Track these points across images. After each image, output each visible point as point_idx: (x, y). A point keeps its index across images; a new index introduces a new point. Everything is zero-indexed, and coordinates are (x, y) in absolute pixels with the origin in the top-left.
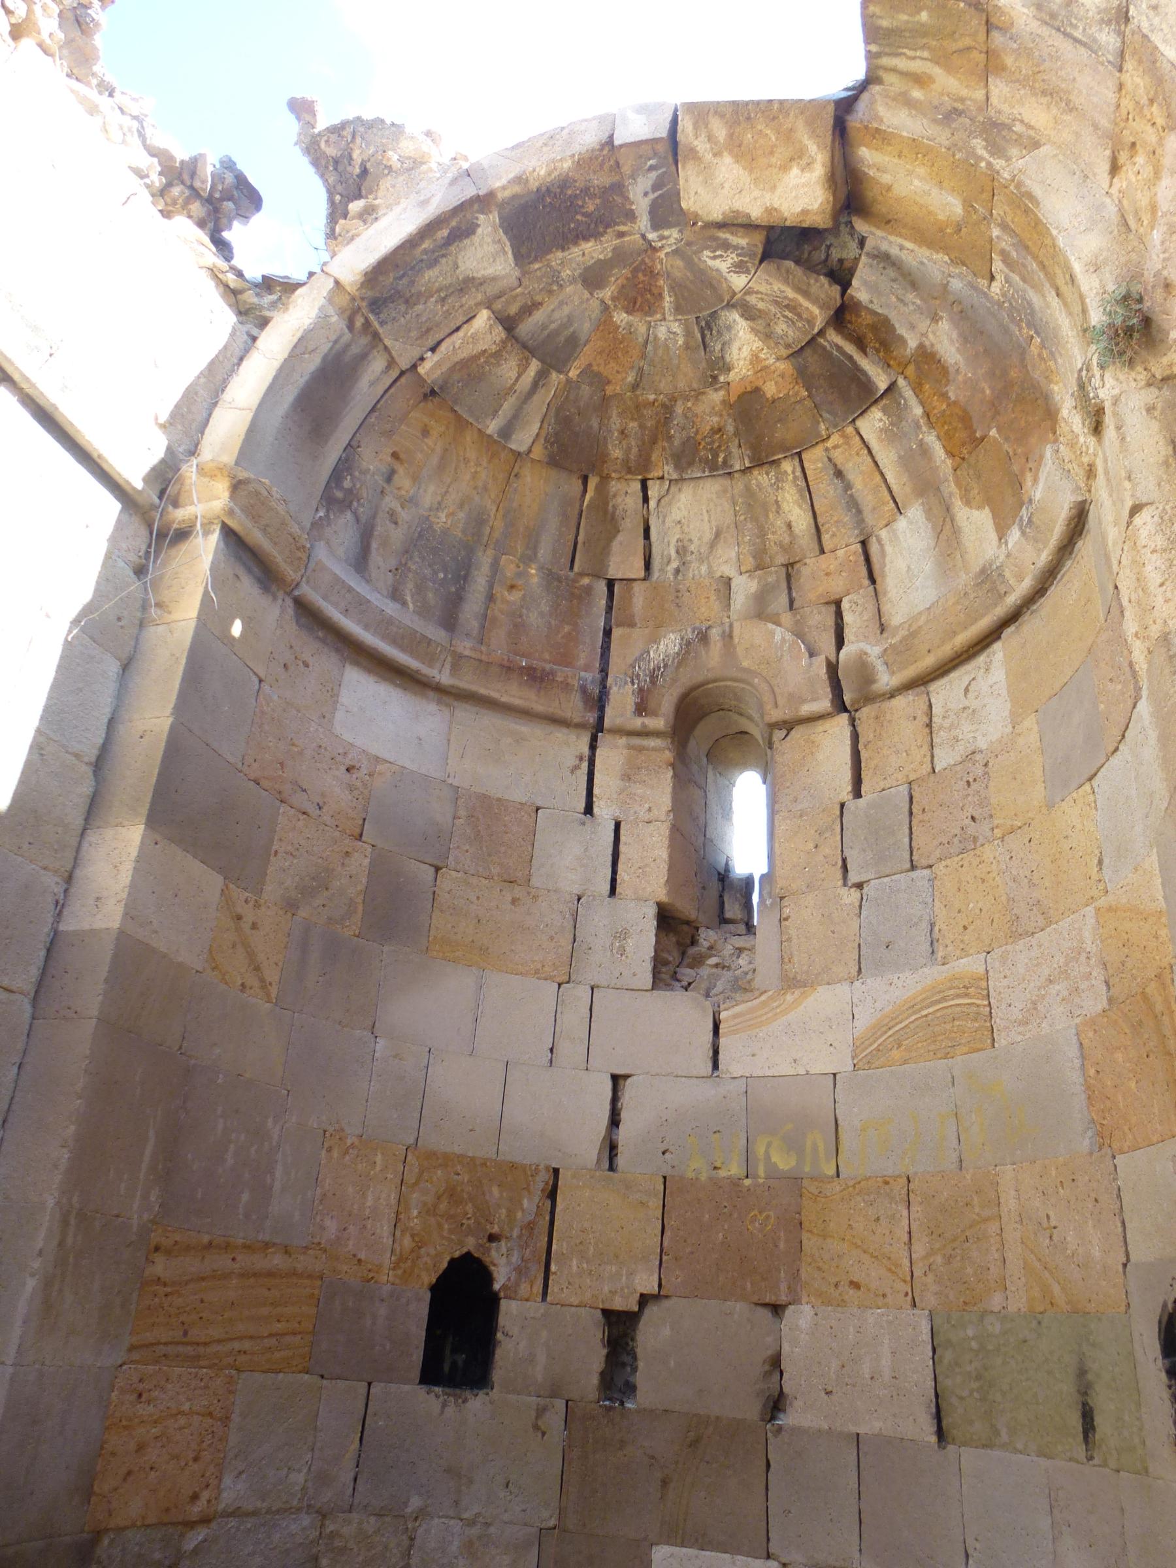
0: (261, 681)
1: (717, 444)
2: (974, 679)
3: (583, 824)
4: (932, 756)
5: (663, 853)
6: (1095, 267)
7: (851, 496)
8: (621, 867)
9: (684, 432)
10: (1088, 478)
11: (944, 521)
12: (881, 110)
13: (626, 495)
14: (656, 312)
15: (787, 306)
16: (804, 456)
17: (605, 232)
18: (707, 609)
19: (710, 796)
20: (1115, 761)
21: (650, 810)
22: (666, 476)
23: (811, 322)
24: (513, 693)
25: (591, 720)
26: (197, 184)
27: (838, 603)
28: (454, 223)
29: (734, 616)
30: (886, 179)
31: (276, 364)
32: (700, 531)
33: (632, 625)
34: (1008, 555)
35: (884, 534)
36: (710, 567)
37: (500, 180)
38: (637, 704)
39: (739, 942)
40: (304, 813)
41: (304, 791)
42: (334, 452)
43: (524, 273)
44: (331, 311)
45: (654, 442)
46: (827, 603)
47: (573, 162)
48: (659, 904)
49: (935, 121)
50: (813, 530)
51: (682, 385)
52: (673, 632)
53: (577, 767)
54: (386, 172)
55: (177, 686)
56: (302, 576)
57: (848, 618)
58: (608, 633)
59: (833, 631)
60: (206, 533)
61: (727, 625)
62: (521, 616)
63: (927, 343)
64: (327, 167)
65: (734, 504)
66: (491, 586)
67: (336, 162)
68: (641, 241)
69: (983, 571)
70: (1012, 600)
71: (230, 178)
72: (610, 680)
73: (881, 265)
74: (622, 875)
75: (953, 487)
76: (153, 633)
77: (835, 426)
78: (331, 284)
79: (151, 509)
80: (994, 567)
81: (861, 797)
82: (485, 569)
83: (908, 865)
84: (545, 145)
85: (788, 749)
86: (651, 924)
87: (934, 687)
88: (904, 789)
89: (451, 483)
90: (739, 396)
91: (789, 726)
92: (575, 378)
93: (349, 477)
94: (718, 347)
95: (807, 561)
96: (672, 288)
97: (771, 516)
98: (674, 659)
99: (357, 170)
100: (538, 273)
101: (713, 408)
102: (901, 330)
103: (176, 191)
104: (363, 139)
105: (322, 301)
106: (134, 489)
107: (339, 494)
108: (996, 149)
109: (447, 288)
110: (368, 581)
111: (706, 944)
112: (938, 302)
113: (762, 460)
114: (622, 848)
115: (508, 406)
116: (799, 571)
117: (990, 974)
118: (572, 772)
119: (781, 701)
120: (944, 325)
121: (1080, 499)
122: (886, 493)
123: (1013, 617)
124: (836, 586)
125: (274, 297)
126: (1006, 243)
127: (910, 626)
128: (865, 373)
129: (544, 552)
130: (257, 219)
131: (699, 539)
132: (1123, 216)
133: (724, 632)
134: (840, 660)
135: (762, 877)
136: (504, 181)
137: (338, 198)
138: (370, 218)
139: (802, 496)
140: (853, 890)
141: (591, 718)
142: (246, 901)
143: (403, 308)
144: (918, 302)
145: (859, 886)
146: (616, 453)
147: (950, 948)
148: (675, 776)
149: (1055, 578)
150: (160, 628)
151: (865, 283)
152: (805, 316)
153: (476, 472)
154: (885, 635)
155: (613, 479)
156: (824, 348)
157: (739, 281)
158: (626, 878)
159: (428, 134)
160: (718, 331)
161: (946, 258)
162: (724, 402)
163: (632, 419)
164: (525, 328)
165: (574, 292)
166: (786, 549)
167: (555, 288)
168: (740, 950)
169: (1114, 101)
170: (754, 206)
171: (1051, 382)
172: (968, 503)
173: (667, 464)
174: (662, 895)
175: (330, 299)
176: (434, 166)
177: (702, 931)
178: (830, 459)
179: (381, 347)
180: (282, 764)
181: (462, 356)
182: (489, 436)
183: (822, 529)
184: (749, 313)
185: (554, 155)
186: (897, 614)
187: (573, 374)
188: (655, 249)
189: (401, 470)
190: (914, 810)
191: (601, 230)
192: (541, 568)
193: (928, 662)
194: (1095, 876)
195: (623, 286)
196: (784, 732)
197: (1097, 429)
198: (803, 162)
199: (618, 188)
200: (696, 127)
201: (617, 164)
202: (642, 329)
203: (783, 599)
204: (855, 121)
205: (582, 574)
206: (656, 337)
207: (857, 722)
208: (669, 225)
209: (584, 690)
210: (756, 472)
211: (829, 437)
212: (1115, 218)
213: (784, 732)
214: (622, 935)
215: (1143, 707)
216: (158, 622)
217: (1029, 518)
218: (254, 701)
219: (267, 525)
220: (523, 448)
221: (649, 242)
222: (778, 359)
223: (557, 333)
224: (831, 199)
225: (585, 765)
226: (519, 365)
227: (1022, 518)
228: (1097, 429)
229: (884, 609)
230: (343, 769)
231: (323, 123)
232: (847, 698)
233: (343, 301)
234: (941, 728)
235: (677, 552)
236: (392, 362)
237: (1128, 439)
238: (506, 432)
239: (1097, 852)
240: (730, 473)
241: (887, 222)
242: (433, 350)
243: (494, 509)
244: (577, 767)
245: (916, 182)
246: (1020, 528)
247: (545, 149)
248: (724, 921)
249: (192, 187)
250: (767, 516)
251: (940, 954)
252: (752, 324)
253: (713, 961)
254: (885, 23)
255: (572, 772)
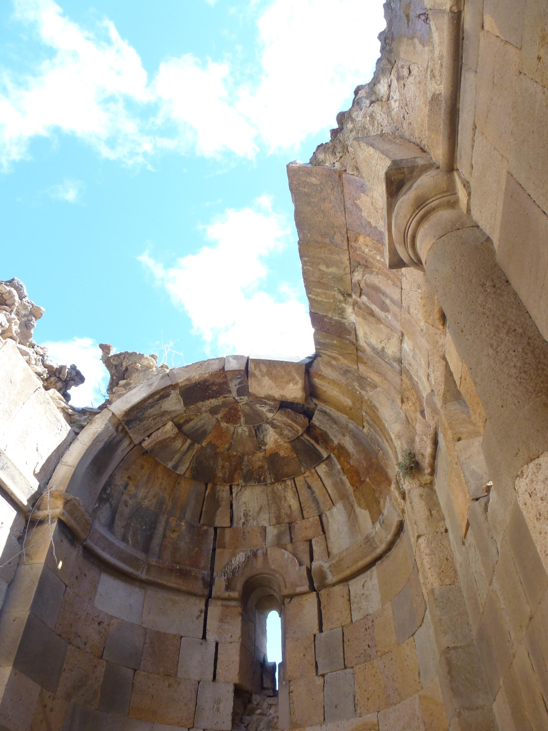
0: (66, 586)
1: (261, 473)
2: (366, 581)
3: (202, 644)
4: (351, 615)
5: (237, 658)
6: (399, 437)
7: (315, 496)
8: (218, 666)
9: (248, 468)
10: (403, 513)
11: (351, 511)
12: (322, 367)
13: (223, 492)
14: (237, 423)
15: (288, 425)
16: (295, 479)
17: (219, 396)
18: (257, 541)
19: (257, 625)
20: (421, 630)
21: (231, 636)
22: (240, 484)
23: (297, 431)
24: (172, 581)
25: (206, 593)
26: (61, 376)
27: (310, 541)
28: (162, 393)
29: (268, 545)
30: (324, 389)
31: (86, 447)
32: (254, 507)
33: (224, 547)
34: (376, 533)
35: (328, 513)
36: (257, 522)
37: (181, 380)
38: (226, 586)
39: (271, 701)
40: (78, 648)
41: (79, 636)
42: (105, 478)
43: (187, 409)
44: (110, 425)
45: (235, 470)
46: (306, 541)
47: (209, 375)
48: (235, 685)
49: (340, 374)
50: (300, 509)
51: (247, 449)
52: (242, 551)
53: (199, 616)
54: (136, 371)
55: (33, 596)
56: (88, 536)
57: (315, 548)
58: (214, 550)
59: (309, 553)
60: (52, 522)
61: (265, 549)
62: (177, 544)
63: (341, 443)
64: (112, 368)
65: (268, 496)
66: (165, 530)
67: (116, 366)
68: (233, 400)
69: (367, 537)
70: (379, 551)
71: (74, 373)
72: (215, 574)
73: (323, 414)
74: (219, 670)
75: (354, 498)
76: (24, 568)
77: (308, 469)
78: (111, 415)
79: (28, 512)
80: (371, 537)
81: (322, 632)
82: (163, 523)
83: (343, 667)
84: (198, 367)
85: (292, 606)
86: (230, 696)
87: (351, 583)
88: (340, 629)
89: (151, 487)
90: (270, 455)
91: (291, 597)
92: (204, 446)
93: (109, 489)
94: (262, 437)
95: (297, 522)
96: (244, 416)
97: (282, 502)
98: (242, 564)
99: (124, 369)
100: (193, 409)
101: (259, 459)
102: (332, 437)
103: (52, 379)
104: (127, 359)
105: (107, 422)
106: (23, 505)
107: (105, 496)
108: (362, 388)
109: (156, 415)
110: (113, 533)
111: (255, 703)
112: (344, 430)
113: (279, 478)
114: (219, 656)
115: (177, 457)
116: (294, 526)
117: (380, 723)
118: (197, 619)
119: (288, 585)
120: (347, 438)
121: (400, 519)
122: (328, 497)
123: (379, 558)
124: (309, 533)
125: (86, 417)
126: (368, 418)
127: (340, 556)
128: (318, 451)
129: (188, 515)
130: (81, 386)
131: (253, 510)
132: (407, 417)
133: (263, 552)
134: (312, 568)
135: (280, 665)
136: (182, 380)
137: (115, 377)
138: (128, 388)
139: (295, 495)
140: (320, 677)
141: (206, 592)
142: (49, 697)
143: (138, 422)
144: (337, 428)
145: (323, 676)
146: (220, 475)
147: (363, 709)
148: (243, 620)
149: (394, 545)
150: (27, 567)
151: (318, 419)
152: (295, 429)
153: (162, 482)
154: (330, 559)
155: (218, 485)
156: (303, 440)
157: (270, 415)
158: (220, 671)
159: (152, 356)
160: (262, 431)
161: (347, 417)
162: (263, 457)
163: (227, 462)
164: (186, 428)
165: (206, 416)
166: (289, 516)
167: (199, 414)
168: (271, 705)
169: (400, 383)
170: (277, 393)
171: (387, 468)
172: (360, 505)
173: (241, 479)
174: (236, 680)
175: (110, 420)
176: (154, 369)
177: (254, 695)
178: (306, 481)
179: (128, 437)
180: (71, 625)
181: (160, 439)
182: (168, 468)
183: (303, 509)
184: (274, 426)
185: (202, 372)
186: (335, 551)
187: (204, 444)
188: (238, 402)
189: (131, 483)
190: (345, 640)
191: (218, 395)
192: (186, 522)
193: (348, 572)
194: (418, 680)
195: (225, 414)
196: (289, 600)
197: (404, 498)
198: (294, 382)
199: (226, 383)
200: (255, 367)
201: (226, 376)
202: (232, 429)
203: (288, 538)
204: (313, 370)
205: (204, 525)
206: (237, 432)
207: (320, 596)
208: (244, 395)
209: (203, 579)
210: (276, 484)
211: (305, 473)
212: (404, 418)
213: (289, 600)
214: (218, 702)
215: (428, 611)
216: (26, 563)
217: (383, 521)
218: (62, 597)
219: (76, 517)
220: (182, 473)
221: (236, 400)
222: (285, 442)
223: (199, 429)
224: (305, 395)
225: (203, 615)
226: (182, 442)
227: (380, 520)
228: (404, 498)
229: (329, 545)
230: (97, 623)
231: (114, 352)
232: (316, 585)
233: (115, 421)
234: (354, 602)
235: (244, 515)
236: (131, 442)
237: (414, 508)
238: (176, 467)
239: (418, 669)
240: (266, 484)
241: (325, 402)
242: (149, 436)
243: (168, 498)
244: (199, 616)
245: (335, 392)
246: (380, 524)
247: (198, 369)
248: (263, 688)
249: (59, 377)
250: (281, 502)
251: (358, 712)
252: (275, 430)
253: (259, 711)
254: (322, 341)
255: (197, 619)
